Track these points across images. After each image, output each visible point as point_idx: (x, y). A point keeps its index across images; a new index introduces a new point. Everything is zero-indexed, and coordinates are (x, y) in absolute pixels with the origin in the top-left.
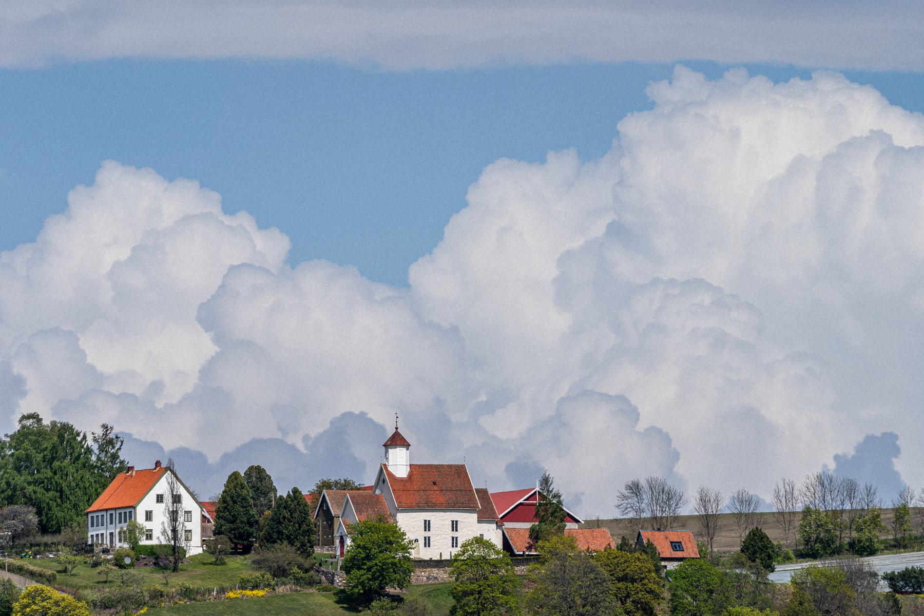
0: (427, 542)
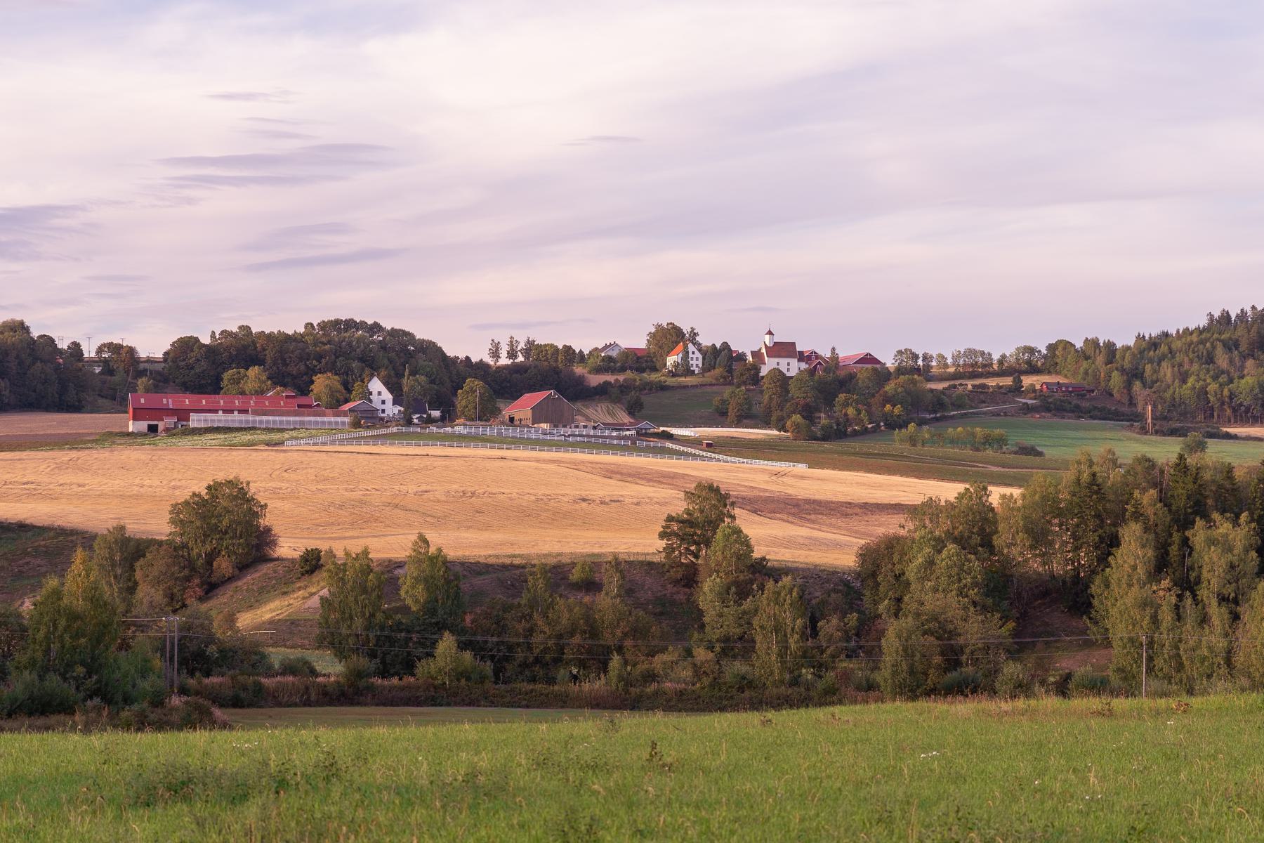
0: (788, 370)
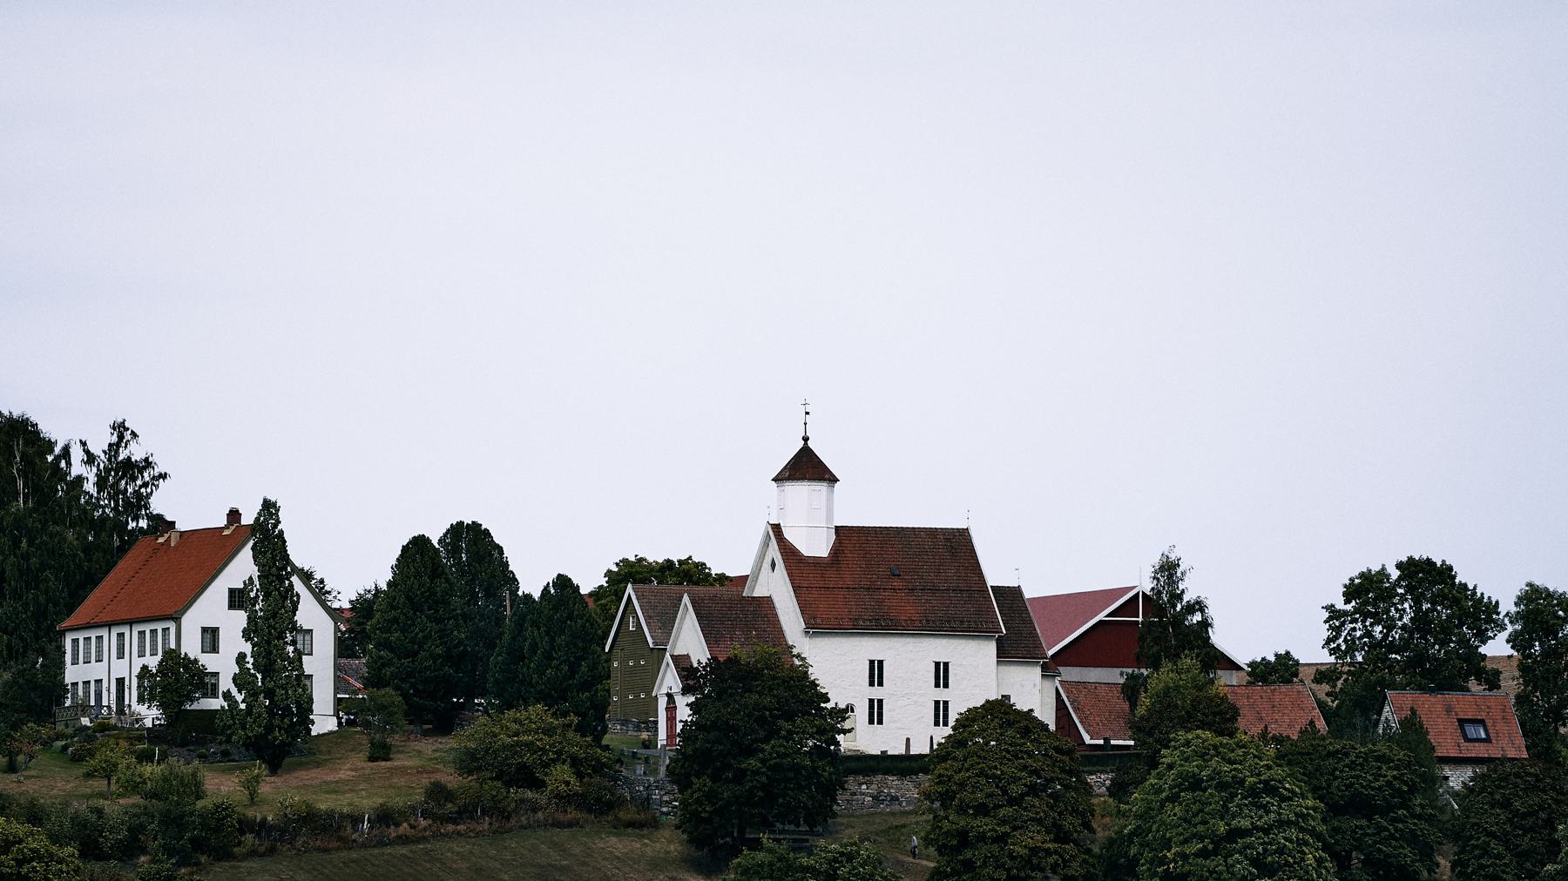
0: (876, 712)
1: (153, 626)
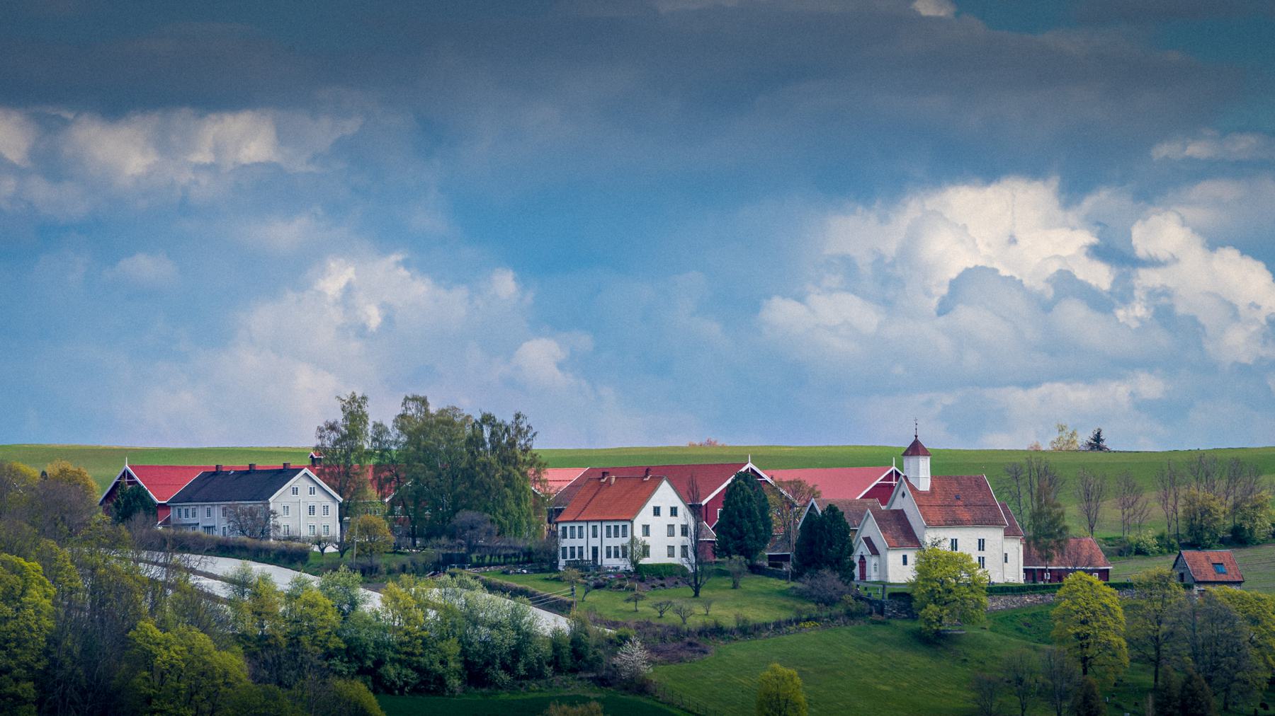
1: (616, 524)
